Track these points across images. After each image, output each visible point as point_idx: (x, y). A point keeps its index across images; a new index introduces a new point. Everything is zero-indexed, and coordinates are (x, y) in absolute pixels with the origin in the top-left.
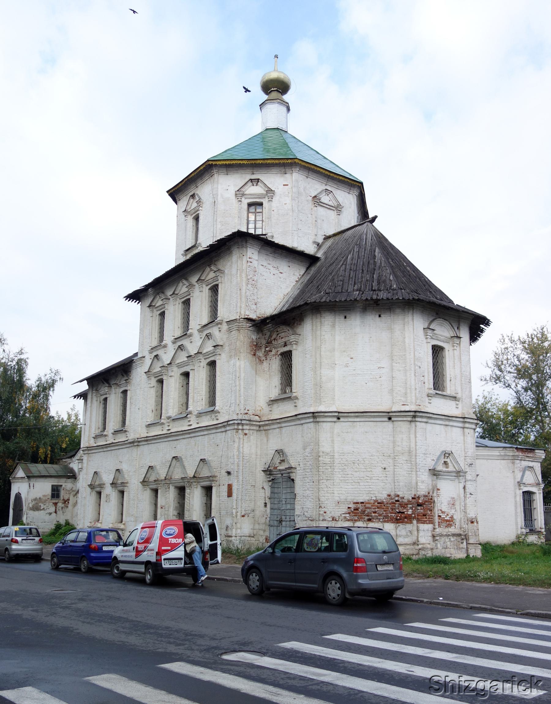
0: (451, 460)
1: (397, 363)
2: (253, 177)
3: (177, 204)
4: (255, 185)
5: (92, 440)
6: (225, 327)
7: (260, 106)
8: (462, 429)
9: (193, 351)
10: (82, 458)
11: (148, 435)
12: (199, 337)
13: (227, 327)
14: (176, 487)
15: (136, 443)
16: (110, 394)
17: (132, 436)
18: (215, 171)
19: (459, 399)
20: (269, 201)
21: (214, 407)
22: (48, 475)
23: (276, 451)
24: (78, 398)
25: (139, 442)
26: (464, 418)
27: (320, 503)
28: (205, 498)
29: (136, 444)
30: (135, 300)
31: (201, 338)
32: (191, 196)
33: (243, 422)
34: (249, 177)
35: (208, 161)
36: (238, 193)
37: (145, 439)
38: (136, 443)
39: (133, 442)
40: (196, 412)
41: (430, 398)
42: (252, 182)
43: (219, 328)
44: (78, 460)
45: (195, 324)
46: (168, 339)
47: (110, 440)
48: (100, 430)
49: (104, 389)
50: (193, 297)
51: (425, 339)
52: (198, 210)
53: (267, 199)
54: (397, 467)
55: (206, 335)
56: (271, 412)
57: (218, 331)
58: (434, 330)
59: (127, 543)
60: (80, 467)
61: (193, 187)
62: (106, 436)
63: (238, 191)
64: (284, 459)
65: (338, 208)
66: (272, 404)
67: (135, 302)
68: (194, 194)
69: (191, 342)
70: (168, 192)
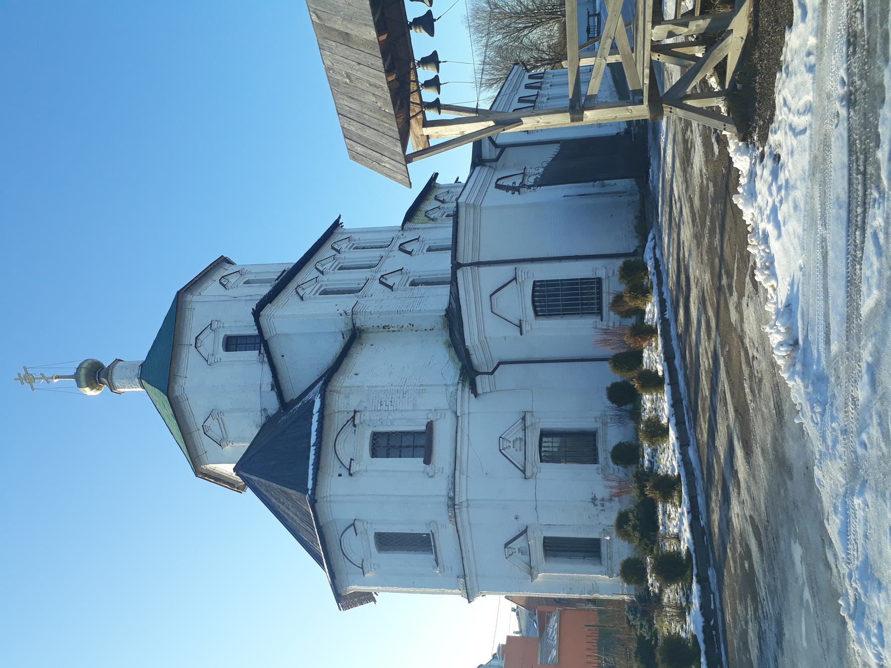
63: (220, 445)
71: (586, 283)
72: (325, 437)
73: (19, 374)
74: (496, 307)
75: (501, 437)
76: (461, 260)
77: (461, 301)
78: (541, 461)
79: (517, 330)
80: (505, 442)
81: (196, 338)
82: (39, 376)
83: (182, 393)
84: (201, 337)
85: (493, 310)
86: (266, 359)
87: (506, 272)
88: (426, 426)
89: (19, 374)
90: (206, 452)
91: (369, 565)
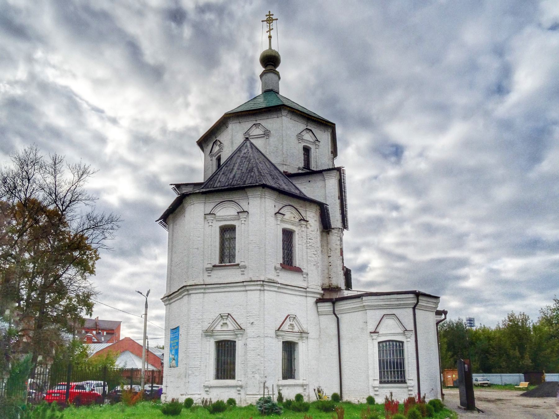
35: (226, 114)
63: (245, 133)
71: (401, 374)
72: (295, 200)
73: (273, 15)
74: (387, 317)
75: (220, 314)
76: (421, 298)
77: (370, 297)
78: (379, 343)
79: (373, 331)
80: (293, 319)
81: (311, 130)
82: (271, 27)
83: (283, 115)
84: (311, 133)
85: (385, 316)
86: (300, 171)
87: (411, 327)
88: (299, 268)
89: (273, 15)
90: (291, 119)
91: (212, 219)
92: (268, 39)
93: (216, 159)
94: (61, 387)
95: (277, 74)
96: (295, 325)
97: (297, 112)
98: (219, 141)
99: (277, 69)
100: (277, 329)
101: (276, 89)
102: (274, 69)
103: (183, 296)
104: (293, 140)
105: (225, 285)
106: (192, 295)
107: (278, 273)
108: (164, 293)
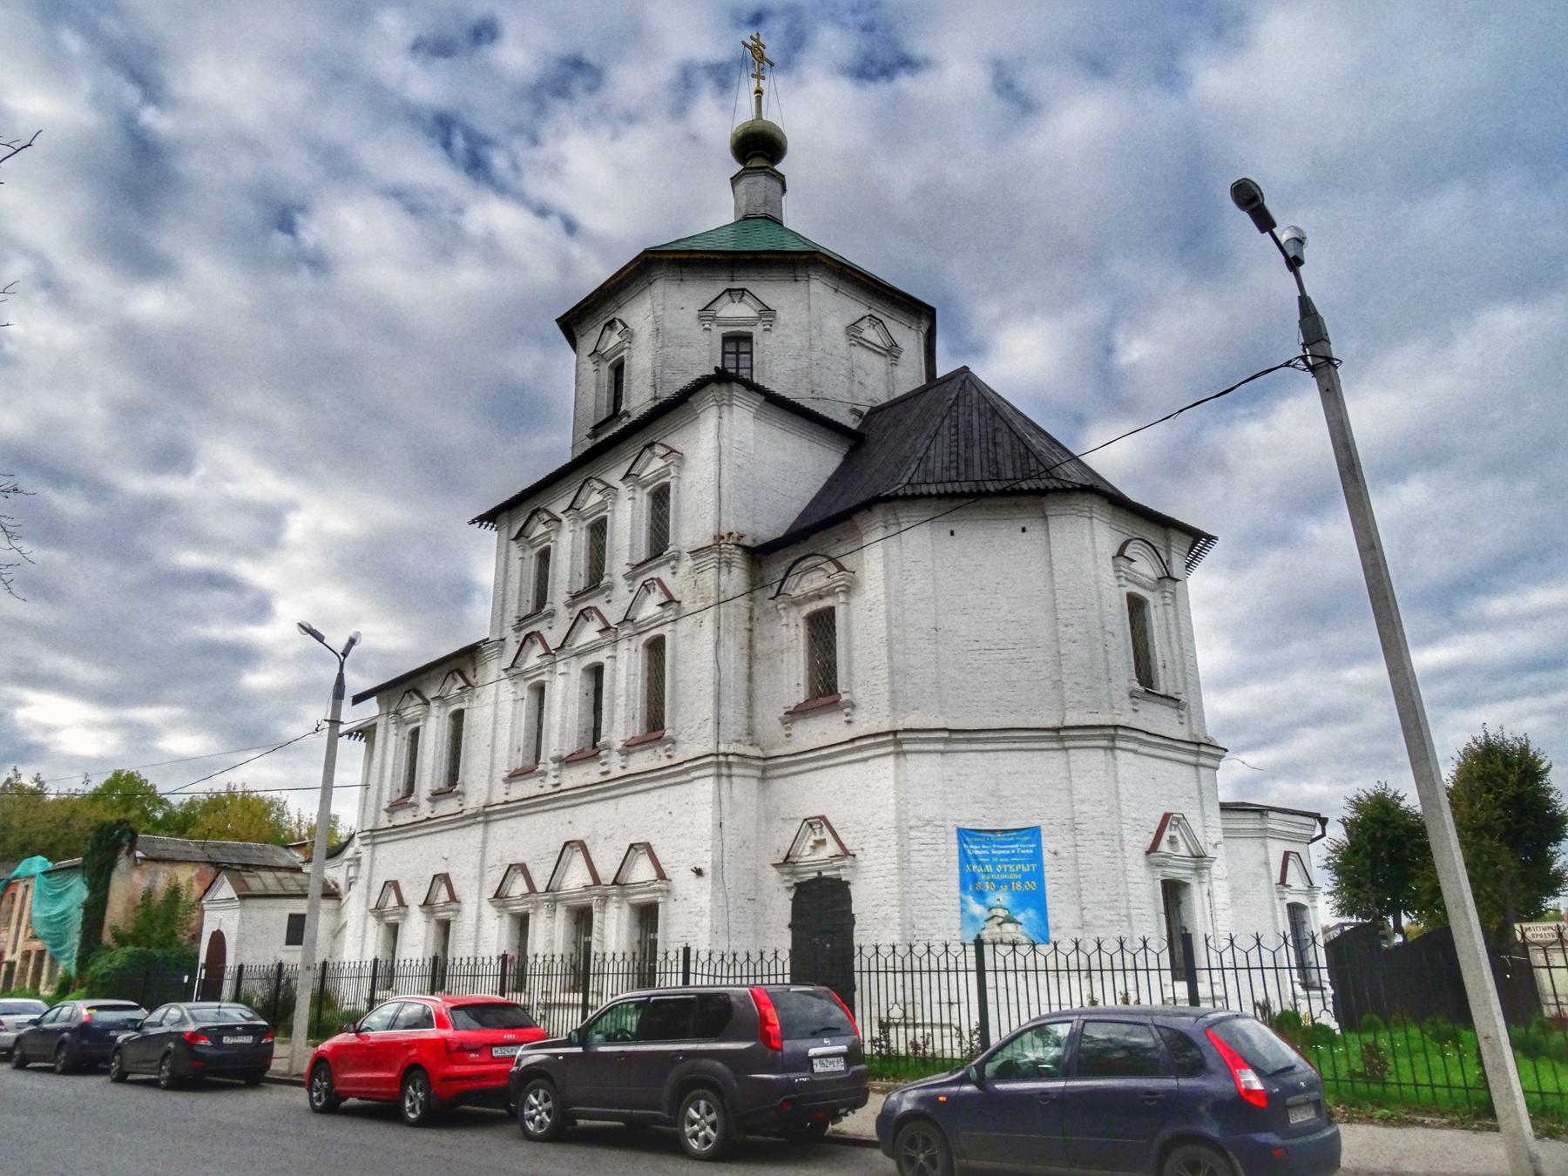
0: (1181, 834)
1: (1067, 626)
2: (736, 285)
3: (575, 350)
4: (736, 300)
5: (384, 817)
6: (687, 564)
7: (731, 179)
8: (1191, 770)
9: (614, 614)
10: (359, 855)
11: (508, 798)
12: (626, 589)
13: (691, 563)
14: (570, 909)
15: (485, 816)
16: (426, 719)
17: (473, 802)
18: (656, 273)
19: (1185, 704)
20: (765, 330)
21: (661, 732)
22: (283, 893)
23: (805, 820)
24: (356, 736)
25: (488, 814)
26: (1199, 744)
27: (916, 932)
28: (638, 930)
29: (479, 819)
30: (485, 523)
31: (631, 591)
32: (606, 325)
33: (731, 758)
34: (722, 286)
35: (646, 252)
36: (704, 313)
37: (505, 807)
38: (485, 816)
39: (475, 816)
40: (619, 745)
41: (1135, 700)
42: (730, 295)
43: (673, 568)
44: (347, 860)
45: (619, 561)
46: (559, 595)
47: (425, 810)
48: (400, 795)
49: (412, 709)
50: (613, 511)
51: (1114, 579)
52: (622, 350)
53: (760, 327)
54: (1083, 849)
55: (643, 584)
56: (789, 739)
57: (669, 575)
58: (1133, 561)
59: (363, 1033)
60: (351, 874)
61: (611, 306)
62: (413, 805)
63: (704, 310)
64: (822, 837)
65: (891, 351)
66: (792, 722)
67: (487, 525)
68: (613, 321)
69: (609, 602)
70: (557, 321)
92: (754, 97)
93: (611, 367)
94: (711, 983)
95: (781, 179)
96: (1179, 838)
97: (888, 292)
98: (620, 321)
99: (778, 167)
100: (1148, 845)
101: (775, 215)
102: (770, 165)
103: (694, 779)
104: (695, 331)
105: (997, 735)
106: (909, 757)
107: (1136, 704)
108: (506, 775)
